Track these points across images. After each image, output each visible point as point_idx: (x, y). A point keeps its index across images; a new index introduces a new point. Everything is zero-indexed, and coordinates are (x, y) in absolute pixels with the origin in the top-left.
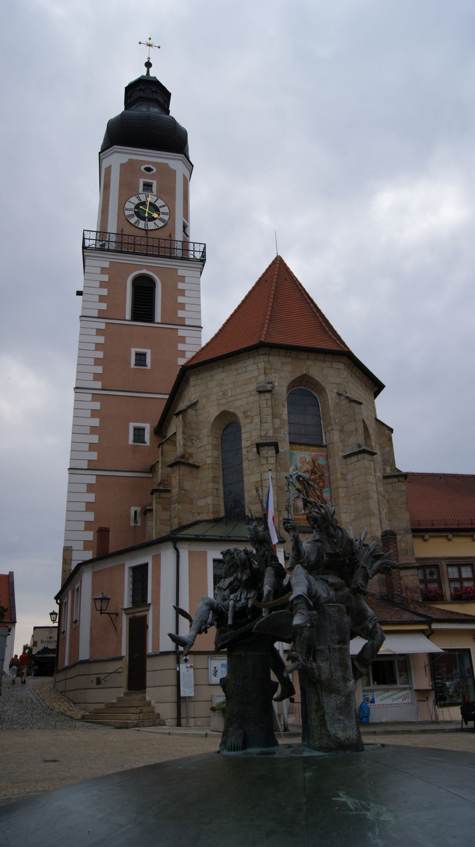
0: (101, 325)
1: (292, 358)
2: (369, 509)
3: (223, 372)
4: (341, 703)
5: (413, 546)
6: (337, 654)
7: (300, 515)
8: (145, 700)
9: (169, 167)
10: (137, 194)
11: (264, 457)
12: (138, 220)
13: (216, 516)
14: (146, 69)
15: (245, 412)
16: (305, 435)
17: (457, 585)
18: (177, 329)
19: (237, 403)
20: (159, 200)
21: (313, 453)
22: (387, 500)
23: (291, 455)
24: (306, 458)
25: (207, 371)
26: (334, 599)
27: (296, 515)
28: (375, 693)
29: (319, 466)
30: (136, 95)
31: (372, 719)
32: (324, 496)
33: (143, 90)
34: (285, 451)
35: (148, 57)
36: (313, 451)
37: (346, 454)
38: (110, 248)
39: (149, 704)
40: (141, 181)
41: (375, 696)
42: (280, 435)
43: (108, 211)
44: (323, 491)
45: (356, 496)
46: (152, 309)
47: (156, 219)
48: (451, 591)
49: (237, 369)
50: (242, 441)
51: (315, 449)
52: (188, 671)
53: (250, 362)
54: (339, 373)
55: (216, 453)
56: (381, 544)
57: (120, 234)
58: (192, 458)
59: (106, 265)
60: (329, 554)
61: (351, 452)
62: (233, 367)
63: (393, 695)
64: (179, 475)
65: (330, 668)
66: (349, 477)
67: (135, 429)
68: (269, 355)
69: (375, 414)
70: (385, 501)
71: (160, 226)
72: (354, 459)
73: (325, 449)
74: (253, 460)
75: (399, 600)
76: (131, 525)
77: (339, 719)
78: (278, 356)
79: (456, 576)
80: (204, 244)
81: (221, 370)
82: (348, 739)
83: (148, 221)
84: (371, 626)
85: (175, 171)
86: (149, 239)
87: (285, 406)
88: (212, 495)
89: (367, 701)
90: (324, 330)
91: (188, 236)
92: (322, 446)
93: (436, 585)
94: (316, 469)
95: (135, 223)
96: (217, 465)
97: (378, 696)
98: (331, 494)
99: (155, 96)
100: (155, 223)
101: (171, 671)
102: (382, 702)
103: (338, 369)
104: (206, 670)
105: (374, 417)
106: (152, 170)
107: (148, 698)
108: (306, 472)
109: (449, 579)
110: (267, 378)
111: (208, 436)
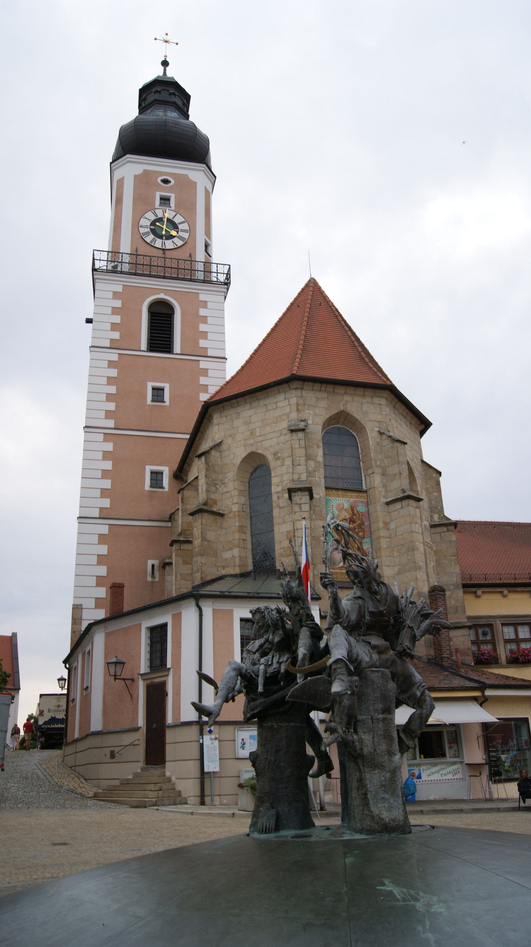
0: (114, 356)
1: (328, 393)
3: (251, 408)
4: (385, 780)
6: (381, 725)
8: (164, 775)
9: (189, 178)
10: (153, 210)
11: (297, 504)
12: (154, 239)
14: (162, 68)
15: (275, 454)
16: (343, 479)
17: (514, 646)
18: (199, 361)
19: (267, 444)
20: (178, 215)
21: (352, 500)
22: (434, 551)
23: (327, 502)
24: (343, 504)
25: (232, 407)
26: (378, 664)
27: (333, 569)
28: (421, 769)
29: (358, 513)
30: (151, 98)
32: (364, 548)
33: (160, 92)
34: (320, 497)
35: (164, 54)
37: (388, 500)
38: (123, 270)
39: (169, 780)
41: (422, 771)
43: (121, 229)
44: (363, 541)
45: (400, 547)
47: (174, 237)
48: (507, 653)
49: (266, 405)
50: (273, 487)
51: (354, 494)
52: (212, 743)
53: (281, 397)
54: (380, 409)
55: (243, 500)
56: (428, 601)
57: (135, 254)
58: (216, 505)
59: (119, 289)
60: (371, 613)
61: (394, 498)
62: (262, 402)
63: (442, 769)
64: (202, 524)
66: (392, 526)
68: (302, 389)
69: (421, 456)
70: (433, 553)
71: (179, 245)
72: (398, 505)
73: (365, 494)
74: (284, 507)
75: (448, 664)
77: (383, 798)
78: (312, 390)
79: (513, 636)
80: (228, 265)
81: (248, 406)
82: (393, 820)
83: (166, 239)
84: (418, 693)
87: (320, 447)
88: (239, 547)
89: (413, 776)
90: (363, 361)
91: (210, 256)
93: (489, 647)
94: (355, 517)
95: (151, 242)
97: (425, 770)
98: (372, 545)
99: (173, 99)
100: (173, 242)
101: (193, 743)
102: (430, 778)
104: (233, 742)
106: (170, 182)
107: (168, 774)
110: (300, 415)
111: (234, 481)
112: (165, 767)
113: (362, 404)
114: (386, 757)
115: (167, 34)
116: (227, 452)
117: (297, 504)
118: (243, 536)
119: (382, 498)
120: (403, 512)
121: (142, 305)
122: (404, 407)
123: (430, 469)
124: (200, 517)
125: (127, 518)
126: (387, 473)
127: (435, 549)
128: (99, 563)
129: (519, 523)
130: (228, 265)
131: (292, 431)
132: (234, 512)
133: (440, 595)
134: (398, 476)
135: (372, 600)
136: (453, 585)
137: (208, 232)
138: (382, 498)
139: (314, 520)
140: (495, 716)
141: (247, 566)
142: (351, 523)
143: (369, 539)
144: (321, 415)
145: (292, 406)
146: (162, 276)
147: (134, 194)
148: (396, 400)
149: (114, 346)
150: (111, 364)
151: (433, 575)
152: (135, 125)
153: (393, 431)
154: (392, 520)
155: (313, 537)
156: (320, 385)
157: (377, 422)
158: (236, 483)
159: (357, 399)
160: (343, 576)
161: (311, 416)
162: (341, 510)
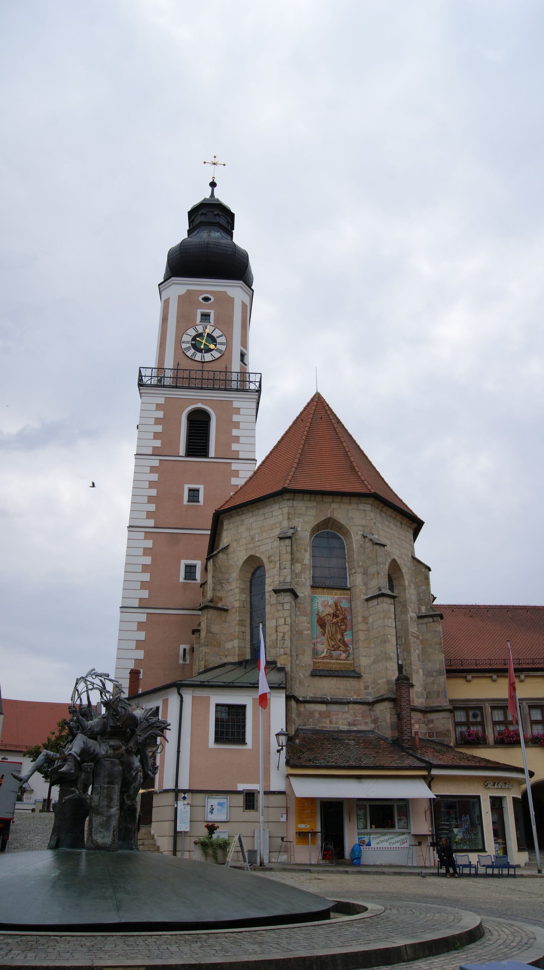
0: (155, 462)
1: (317, 502)
2: (386, 653)
3: (252, 516)
4: (103, 821)
5: (445, 688)
6: (105, 791)
8: (150, 833)
9: (227, 295)
10: (194, 326)
11: (280, 603)
12: (194, 353)
13: (241, 659)
14: (211, 188)
15: (269, 558)
16: (330, 578)
17: (502, 728)
18: (231, 463)
19: (263, 548)
20: (217, 330)
21: (336, 597)
22: (421, 641)
23: (312, 600)
24: (328, 601)
25: (238, 515)
26: (112, 756)
27: (315, 658)
28: (371, 837)
30: (198, 220)
31: (364, 861)
32: (346, 639)
33: (205, 214)
34: (305, 595)
35: (213, 176)
36: (336, 594)
37: (368, 597)
38: (165, 384)
39: (153, 837)
40: (199, 312)
41: (372, 839)
42: (300, 579)
43: (165, 345)
44: (345, 634)
45: (375, 639)
46: (206, 443)
47: (213, 350)
49: (264, 514)
50: (266, 586)
51: (338, 592)
52: (185, 808)
53: (276, 507)
54: (365, 514)
55: (244, 597)
56: (395, 688)
57: (176, 369)
58: (222, 601)
59: (162, 401)
60: (111, 727)
61: (372, 595)
62: (261, 511)
63: (391, 838)
64: (207, 619)
65: (99, 799)
66: (370, 620)
67: (187, 566)
68: (294, 500)
69: (413, 552)
70: (419, 642)
71: (217, 357)
72: (375, 602)
73: (348, 592)
74: (274, 605)
75: (408, 745)
76: (180, 663)
77: (100, 831)
78: (303, 500)
79: (501, 718)
80: (259, 374)
81: (250, 514)
82: (104, 844)
83: (205, 353)
84: (134, 774)
85: (234, 298)
86: (204, 372)
87: (308, 551)
88: (238, 639)
89: (363, 843)
90: (353, 470)
91: (246, 365)
92: (344, 588)
93: (480, 728)
94: (338, 612)
95: (192, 356)
96: (245, 609)
97: (374, 839)
98: (352, 637)
99: (217, 219)
100: (211, 354)
101: (170, 807)
102: (379, 846)
103: (365, 510)
104: (203, 808)
105: (410, 555)
107: (152, 832)
108: (328, 616)
109: (493, 721)
110: (291, 523)
111: (237, 580)
112: (151, 827)
113: (348, 510)
114: (106, 809)
115: (215, 157)
116: (232, 555)
117: (280, 603)
118: (243, 629)
119: (362, 595)
120: (379, 608)
121: (183, 412)
122: (391, 510)
123: (420, 564)
124: (206, 612)
125: (163, 607)
126: (368, 572)
127: (421, 638)
128: (138, 647)
129: (535, 607)
130: (259, 374)
131: (281, 538)
132: (236, 608)
133: (404, 683)
134: (376, 576)
135: (113, 719)
136: (436, 671)
137: (244, 342)
138: (362, 595)
139: (298, 616)
140: (434, 792)
141: (245, 655)
142: (335, 617)
143: (351, 632)
144: (309, 523)
145: (285, 515)
146: (199, 387)
147: (178, 313)
148: (382, 505)
149: (155, 453)
150: (153, 469)
151: (417, 662)
152: (183, 245)
153: (378, 533)
154: (371, 615)
155: (297, 631)
156: (309, 495)
157: (362, 526)
158: (238, 582)
159: (343, 506)
160: (324, 665)
161: (300, 524)
162: (325, 606)
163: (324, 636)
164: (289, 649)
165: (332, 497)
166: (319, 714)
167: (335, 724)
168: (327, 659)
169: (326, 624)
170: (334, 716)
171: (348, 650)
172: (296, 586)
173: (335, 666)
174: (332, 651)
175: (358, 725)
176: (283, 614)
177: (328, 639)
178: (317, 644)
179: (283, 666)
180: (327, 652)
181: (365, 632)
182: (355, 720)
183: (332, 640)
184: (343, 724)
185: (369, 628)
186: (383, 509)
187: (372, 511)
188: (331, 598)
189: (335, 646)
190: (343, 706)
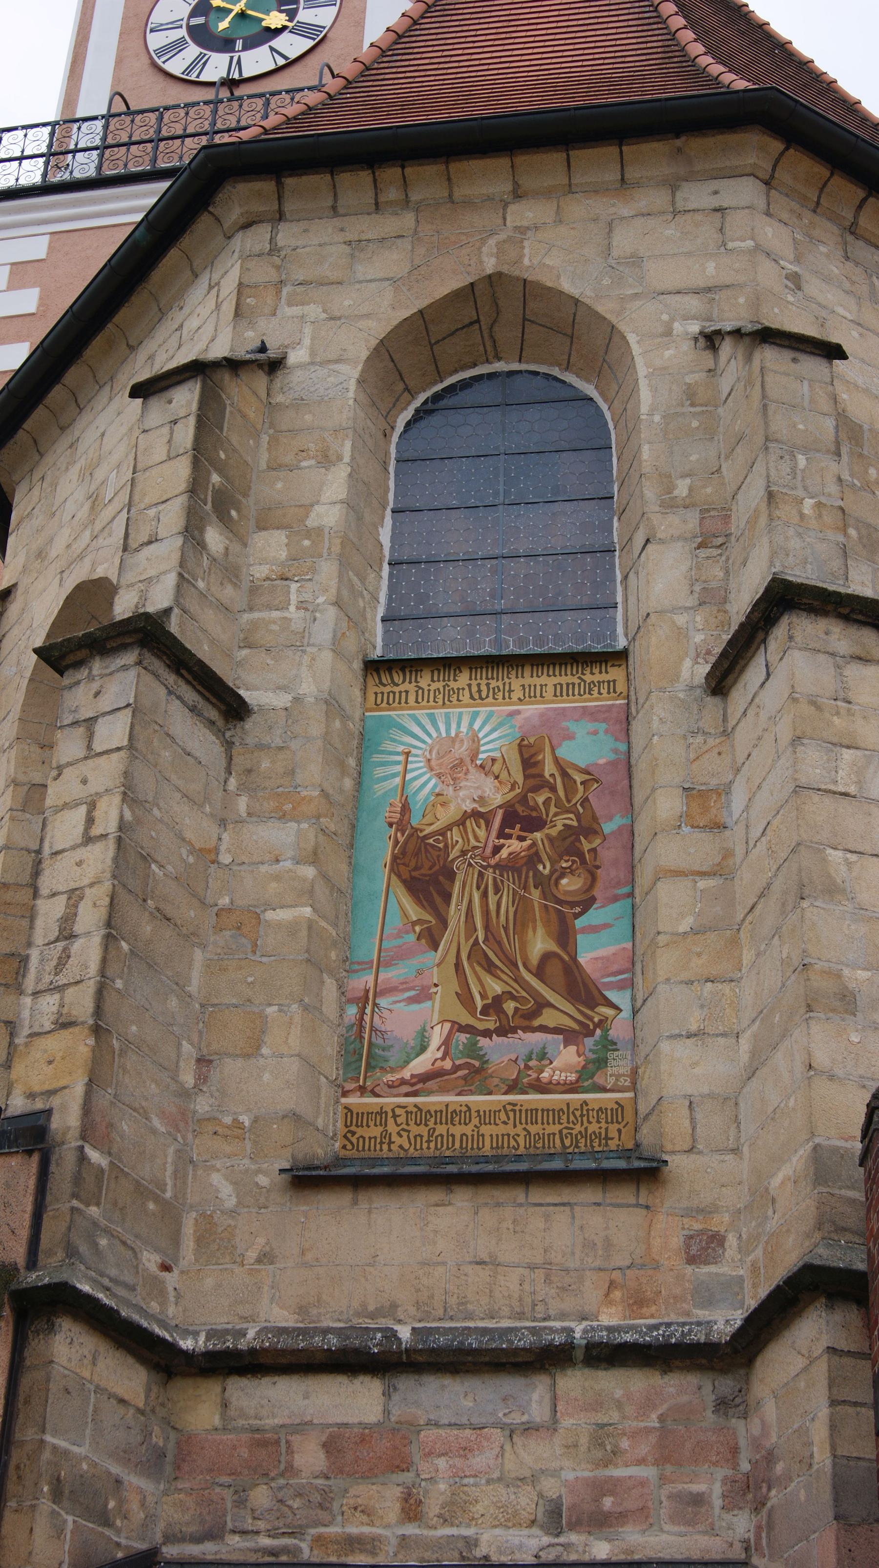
7: (391, 1085)
12: (201, 56)
21: (531, 710)
24: (475, 740)
27: (362, 1090)
29: (564, 774)
32: (583, 959)
34: (297, 700)
36: (531, 695)
42: (275, 614)
44: (579, 923)
47: (278, 31)
51: (548, 680)
73: (615, 673)
83: (245, 48)
87: (340, 458)
100: (272, 49)
108: (470, 824)
113: (610, 224)
119: (687, 663)
138: (687, 663)
139: (239, 821)
143: (620, 908)
144: (367, 316)
161: (308, 330)
163: (435, 946)
164: (88, 991)
165: (502, 163)
166: (331, 1446)
167: (446, 1521)
168: (443, 1090)
169: (451, 876)
170: (442, 1463)
171: (602, 1023)
172: (245, 652)
173: (502, 1129)
174: (487, 1034)
175: (622, 1517)
176: (84, 782)
177: (458, 966)
178: (383, 1002)
179: (39, 1105)
180: (446, 1042)
181: (702, 884)
182: (602, 1488)
183: (490, 967)
184: (511, 1520)
185: (728, 854)
186: (863, 221)
187: (768, 214)
188: (494, 721)
189: (510, 1006)
190: (510, 1384)
